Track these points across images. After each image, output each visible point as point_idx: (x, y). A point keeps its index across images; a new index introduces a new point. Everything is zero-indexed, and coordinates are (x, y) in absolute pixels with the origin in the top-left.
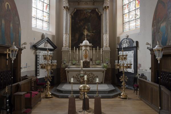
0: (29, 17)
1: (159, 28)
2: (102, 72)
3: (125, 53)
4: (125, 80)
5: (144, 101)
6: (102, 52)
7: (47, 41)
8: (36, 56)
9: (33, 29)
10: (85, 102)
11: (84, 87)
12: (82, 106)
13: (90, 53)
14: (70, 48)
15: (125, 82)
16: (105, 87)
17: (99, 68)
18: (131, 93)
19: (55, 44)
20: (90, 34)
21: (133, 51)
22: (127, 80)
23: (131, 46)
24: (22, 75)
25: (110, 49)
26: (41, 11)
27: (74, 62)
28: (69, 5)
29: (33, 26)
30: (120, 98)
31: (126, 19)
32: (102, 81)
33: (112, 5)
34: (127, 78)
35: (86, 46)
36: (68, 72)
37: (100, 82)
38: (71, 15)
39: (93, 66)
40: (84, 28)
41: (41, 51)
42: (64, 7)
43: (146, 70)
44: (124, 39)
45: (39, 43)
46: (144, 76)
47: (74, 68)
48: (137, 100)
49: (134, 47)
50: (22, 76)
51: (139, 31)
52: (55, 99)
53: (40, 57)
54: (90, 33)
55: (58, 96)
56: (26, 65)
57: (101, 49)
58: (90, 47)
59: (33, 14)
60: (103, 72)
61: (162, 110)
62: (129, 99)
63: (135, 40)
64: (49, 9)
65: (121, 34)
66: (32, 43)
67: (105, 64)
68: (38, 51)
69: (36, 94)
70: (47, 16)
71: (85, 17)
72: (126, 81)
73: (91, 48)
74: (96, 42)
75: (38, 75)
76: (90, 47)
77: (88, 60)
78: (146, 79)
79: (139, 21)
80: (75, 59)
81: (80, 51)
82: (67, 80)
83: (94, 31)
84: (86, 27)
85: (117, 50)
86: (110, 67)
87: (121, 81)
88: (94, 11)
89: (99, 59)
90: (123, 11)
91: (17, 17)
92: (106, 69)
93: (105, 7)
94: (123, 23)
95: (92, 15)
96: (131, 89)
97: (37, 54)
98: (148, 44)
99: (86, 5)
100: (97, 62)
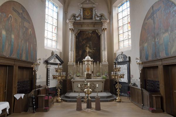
0: (43, 37)
1: (144, 47)
2: (101, 82)
3: (120, 66)
4: (119, 87)
5: (134, 103)
6: (102, 65)
7: (56, 57)
8: (47, 69)
9: (45, 48)
10: (88, 104)
11: (88, 90)
12: (86, 106)
14: (75, 63)
15: (120, 89)
16: (105, 94)
17: (99, 79)
18: (125, 99)
19: (62, 60)
20: (91, 51)
21: (127, 65)
22: (121, 87)
23: (125, 61)
24: (37, 84)
25: (108, 63)
26: (52, 33)
27: (78, 75)
28: (74, 27)
29: (45, 45)
30: (116, 101)
31: (121, 39)
32: (102, 90)
33: (110, 27)
34: (121, 86)
35: (88, 61)
36: (73, 82)
37: (100, 91)
38: (75, 35)
39: (94, 78)
40: (87, 46)
41: (51, 66)
42: (70, 29)
43: (137, 80)
44: (119, 55)
45: (50, 58)
46: (135, 84)
47: (78, 79)
48: (130, 103)
49: (127, 61)
50: (38, 85)
51: (130, 49)
52: (64, 103)
53: (50, 70)
54: (92, 50)
55: (66, 101)
56: (40, 77)
57: (101, 63)
58: (91, 61)
59: (46, 35)
60: (103, 82)
61: (145, 107)
62: (123, 102)
63: (128, 56)
64: (57, 30)
65: (117, 51)
66: (44, 59)
67: (104, 76)
68: (49, 65)
69: (51, 98)
70: (55, 36)
71: (87, 37)
72: (120, 88)
73: (92, 63)
74: (97, 57)
75: (49, 85)
76: (91, 61)
77: (90, 73)
78: (137, 87)
79: (131, 40)
80: (79, 72)
81: (83, 65)
82: (72, 89)
83: (95, 49)
84: (88, 45)
85: (114, 64)
86: (108, 78)
87: (116, 88)
88: (94, 32)
89: (99, 71)
90: (118, 31)
91: (35, 39)
92: (105, 80)
93: (104, 29)
94: (119, 42)
95: (93, 35)
96: (126, 96)
97: (48, 68)
98: (137, 59)
99: (88, 27)
100: (97, 74)
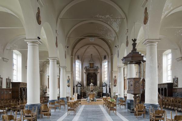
13: (93, 87)
35: (92, 85)
45: (78, 84)
74: (95, 84)
77: (92, 90)
